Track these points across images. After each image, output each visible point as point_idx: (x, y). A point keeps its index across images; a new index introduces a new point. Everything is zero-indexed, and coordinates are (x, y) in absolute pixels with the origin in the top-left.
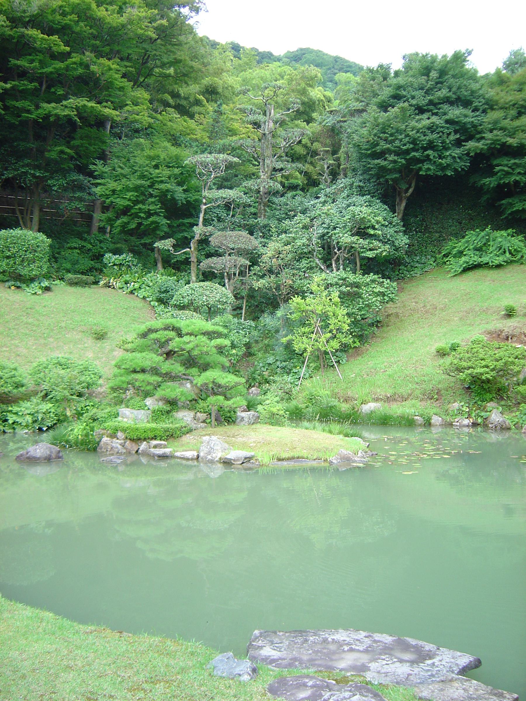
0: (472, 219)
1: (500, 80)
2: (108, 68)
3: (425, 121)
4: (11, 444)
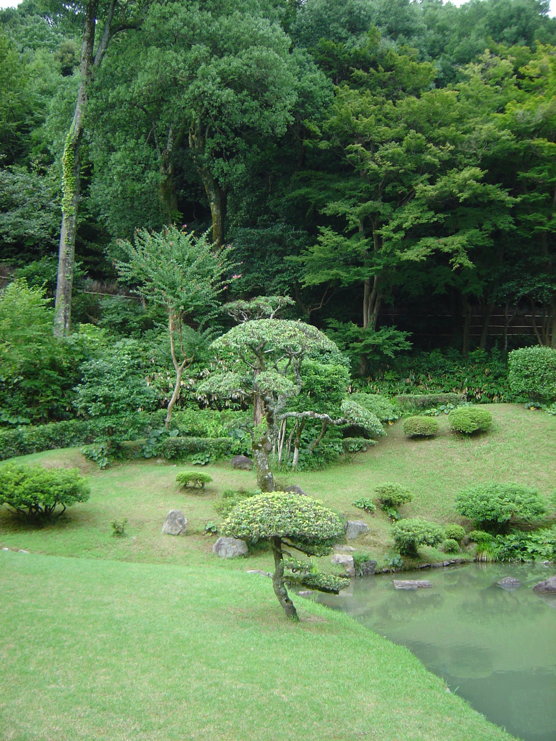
4: (530, 575)
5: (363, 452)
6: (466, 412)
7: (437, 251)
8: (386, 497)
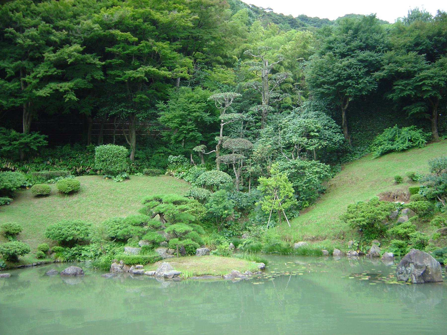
0: (392, 120)
1: (399, 30)
2: (163, 47)
3: (346, 62)
5: (8, 205)
6: (69, 180)
7: (57, 90)
8: (362, 218)
